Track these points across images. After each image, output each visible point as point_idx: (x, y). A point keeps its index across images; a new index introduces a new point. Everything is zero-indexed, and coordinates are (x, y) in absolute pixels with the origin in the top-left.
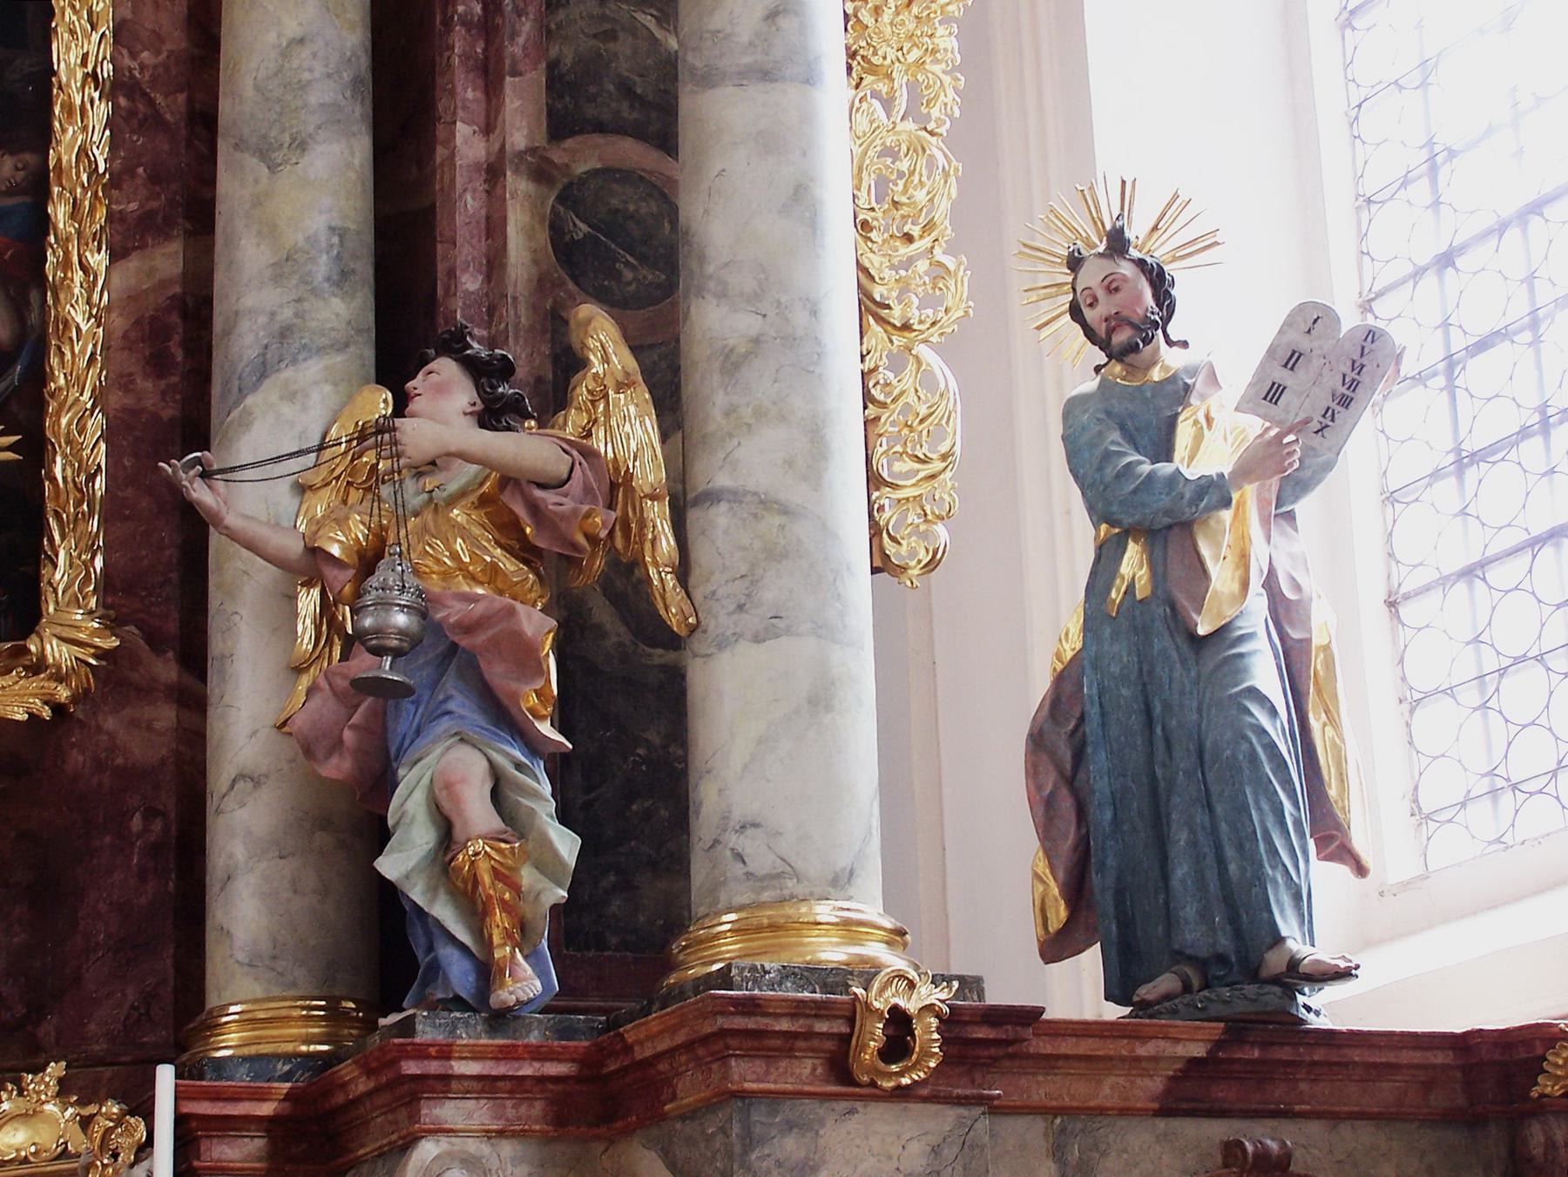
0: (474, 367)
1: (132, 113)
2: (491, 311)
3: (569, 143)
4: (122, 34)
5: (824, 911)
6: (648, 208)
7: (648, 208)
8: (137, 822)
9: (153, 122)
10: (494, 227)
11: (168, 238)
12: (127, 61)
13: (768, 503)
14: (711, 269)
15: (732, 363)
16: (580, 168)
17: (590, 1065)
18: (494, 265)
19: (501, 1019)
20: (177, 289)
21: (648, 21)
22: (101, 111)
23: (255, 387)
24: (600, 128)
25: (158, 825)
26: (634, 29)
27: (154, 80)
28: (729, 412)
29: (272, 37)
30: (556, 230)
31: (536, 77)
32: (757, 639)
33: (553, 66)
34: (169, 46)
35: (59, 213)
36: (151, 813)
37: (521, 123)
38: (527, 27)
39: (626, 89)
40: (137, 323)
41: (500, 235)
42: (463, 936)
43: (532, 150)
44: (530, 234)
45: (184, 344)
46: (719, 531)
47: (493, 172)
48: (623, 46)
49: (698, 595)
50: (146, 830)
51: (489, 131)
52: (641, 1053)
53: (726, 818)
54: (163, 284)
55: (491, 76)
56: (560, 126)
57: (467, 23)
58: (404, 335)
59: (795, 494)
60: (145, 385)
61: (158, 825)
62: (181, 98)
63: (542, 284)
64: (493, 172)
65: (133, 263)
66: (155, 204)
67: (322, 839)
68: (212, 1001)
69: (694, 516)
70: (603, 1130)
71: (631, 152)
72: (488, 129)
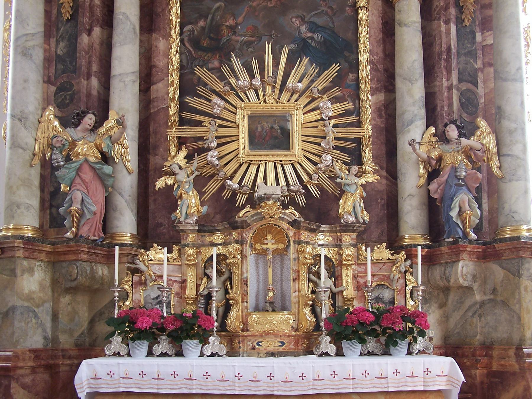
0: (458, 127)
1: (373, 68)
2: (449, 114)
3: (462, 84)
4: (371, 52)
5: (525, 227)
6: (473, 97)
7: (473, 97)
8: (379, 200)
9: (377, 70)
10: (450, 98)
11: (381, 92)
12: (372, 58)
13: (518, 157)
14: (507, 115)
15: (511, 132)
16: (463, 89)
17: (484, 251)
18: (450, 105)
19: (470, 242)
20: (383, 102)
21: (472, 61)
22: (369, 68)
23: (410, 125)
24: (466, 81)
25: (383, 201)
26: (470, 63)
27: (377, 62)
28: (511, 141)
29: (410, 59)
30: (460, 100)
31: (457, 71)
32: (517, 181)
33: (459, 69)
34: (379, 55)
35: (363, 87)
36: (382, 199)
37: (455, 80)
38: (455, 61)
39: (469, 74)
40: (376, 108)
41: (452, 103)
42: (461, 227)
43: (456, 85)
44: (457, 100)
45: (385, 113)
46: (508, 162)
47: (450, 88)
48: (468, 66)
49: (504, 172)
50: (381, 202)
51: (449, 81)
52: (497, 249)
53: (510, 210)
54: (381, 101)
55: (449, 71)
56: (460, 81)
57: (444, 60)
58: (431, 118)
59: (521, 156)
60: (378, 120)
61: (383, 201)
62: (382, 66)
63: (459, 110)
64: (450, 88)
65: (375, 97)
66: (378, 86)
67: (424, 207)
68: (401, 234)
69: (501, 158)
70: (484, 261)
71: (471, 86)
72: (448, 80)
